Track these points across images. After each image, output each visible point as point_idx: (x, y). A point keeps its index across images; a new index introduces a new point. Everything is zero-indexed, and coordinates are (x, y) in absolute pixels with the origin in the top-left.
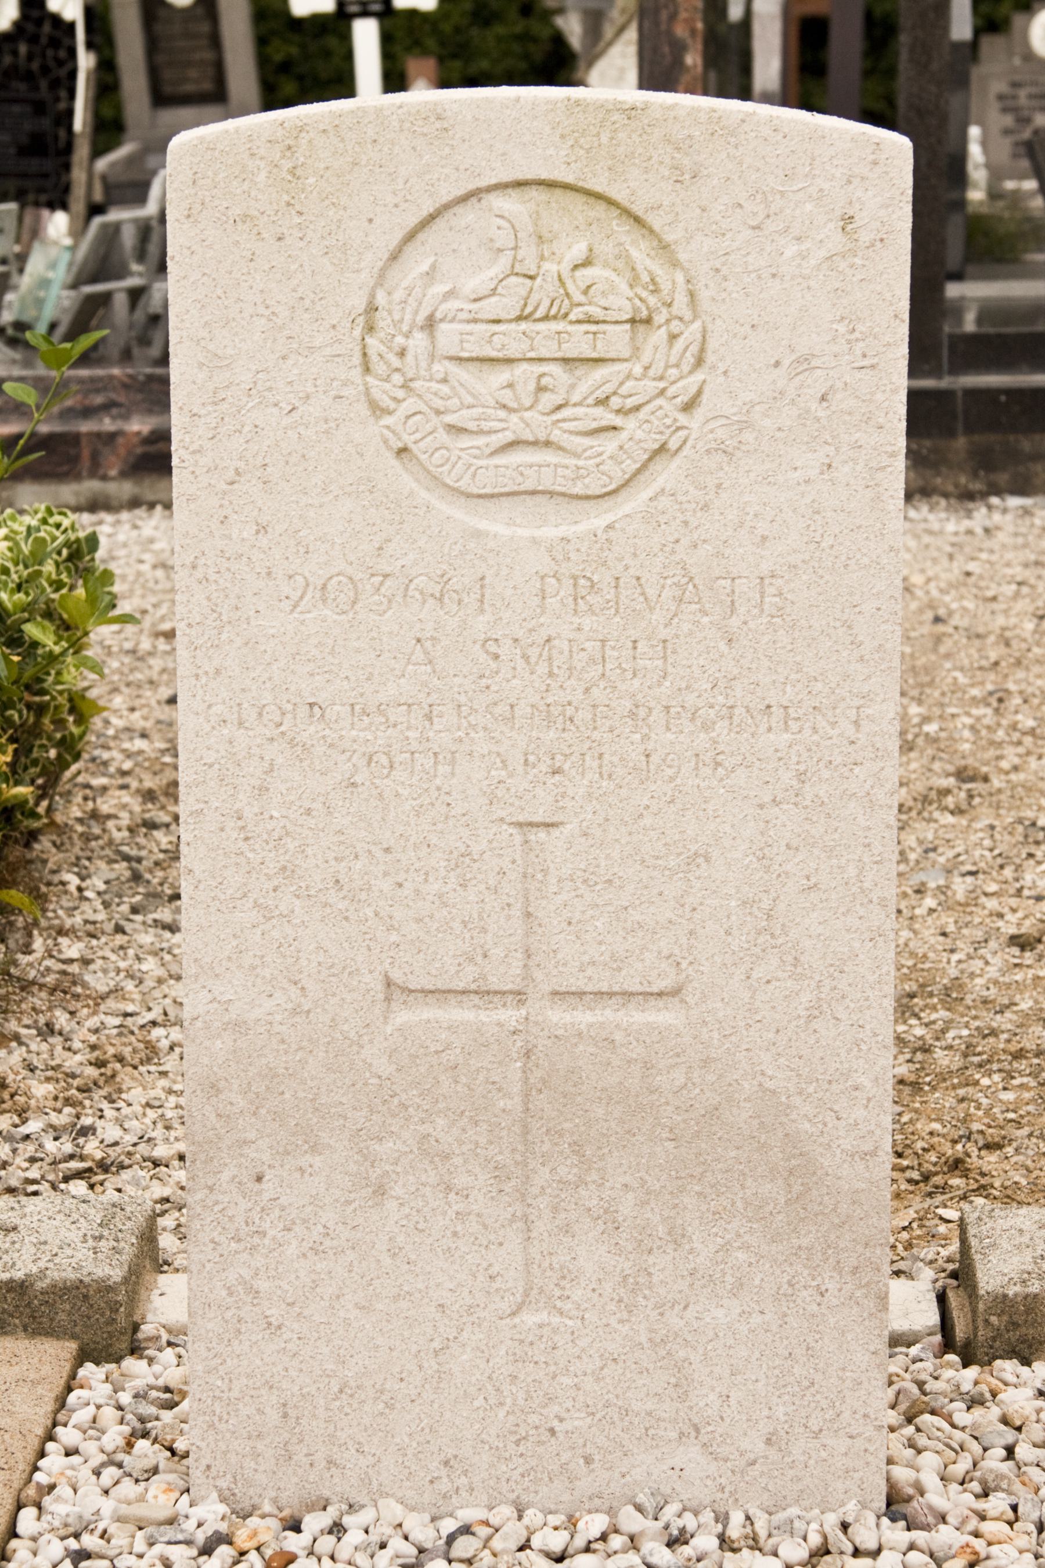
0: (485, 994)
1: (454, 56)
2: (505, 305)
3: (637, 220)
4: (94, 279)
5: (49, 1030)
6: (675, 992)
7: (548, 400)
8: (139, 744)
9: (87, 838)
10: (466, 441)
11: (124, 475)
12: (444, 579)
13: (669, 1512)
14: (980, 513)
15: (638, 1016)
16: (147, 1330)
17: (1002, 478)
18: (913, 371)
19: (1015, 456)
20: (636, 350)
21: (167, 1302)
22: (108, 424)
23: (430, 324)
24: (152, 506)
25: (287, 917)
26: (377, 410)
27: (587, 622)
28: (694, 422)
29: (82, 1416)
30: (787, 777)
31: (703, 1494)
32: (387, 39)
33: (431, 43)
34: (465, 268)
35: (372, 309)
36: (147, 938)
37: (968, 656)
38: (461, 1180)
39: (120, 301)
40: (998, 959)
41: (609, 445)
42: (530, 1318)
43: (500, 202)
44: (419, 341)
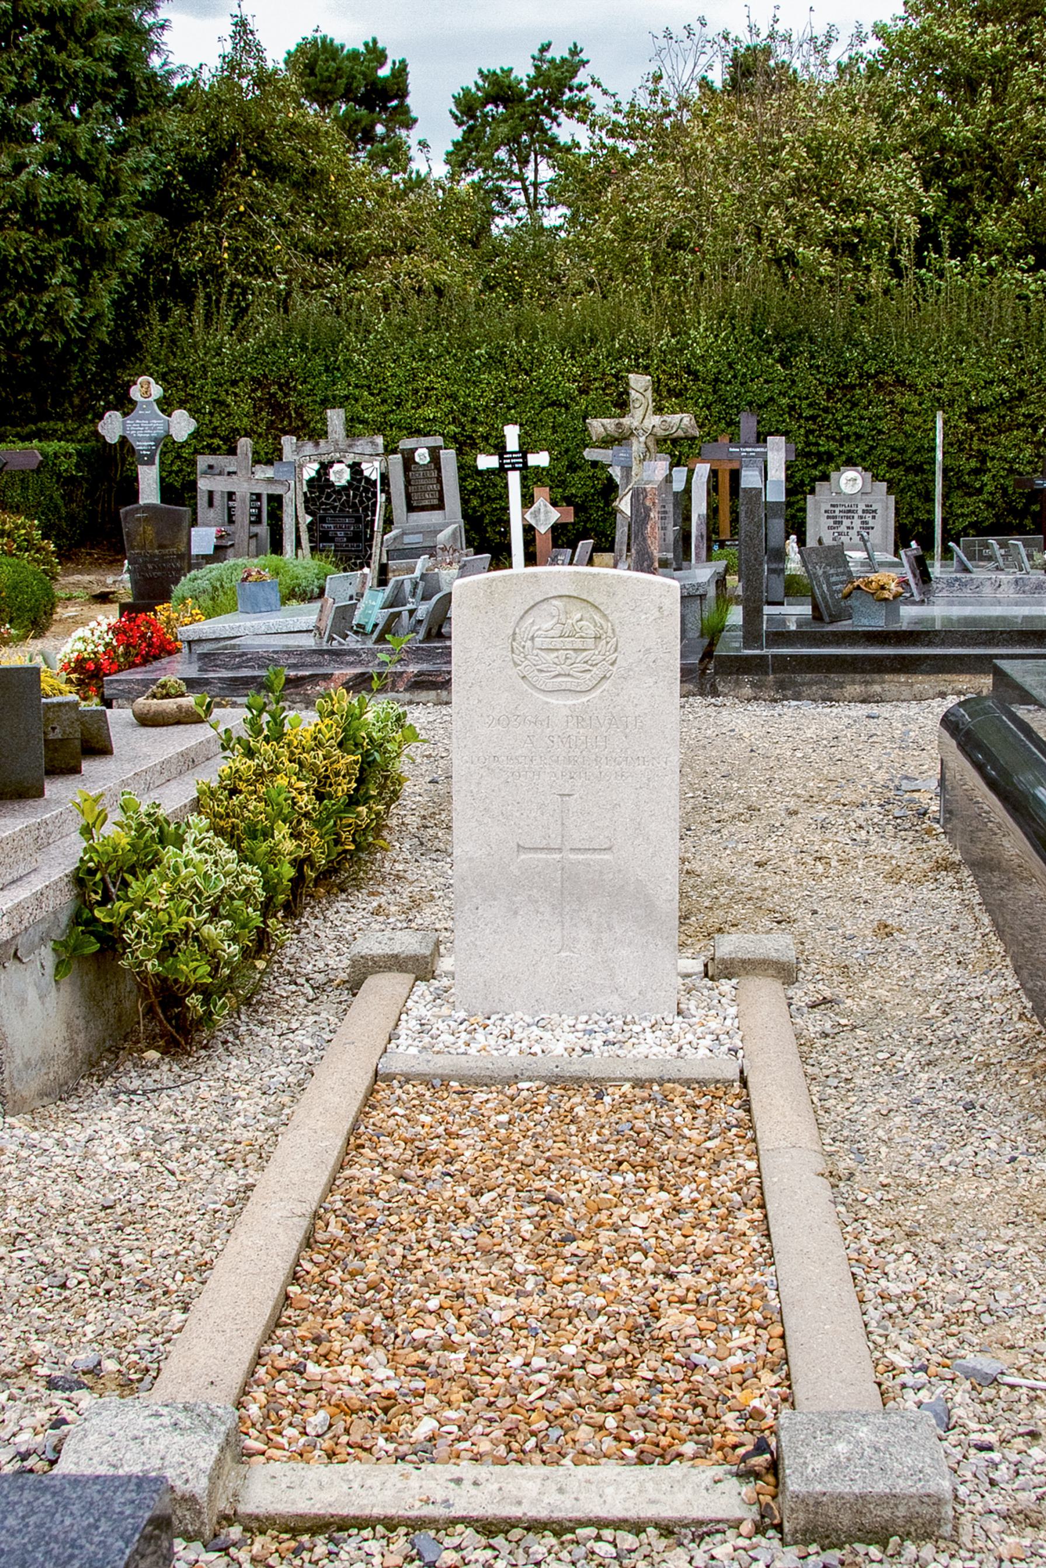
0: (549, 849)
1: (558, 487)
2: (556, 632)
4: (391, 606)
5: (394, 892)
6: (610, 849)
7: (569, 662)
8: (418, 798)
9: (400, 832)
11: (406, 690)
12: (536, 717)
13: (608, 1015)
14: (779, 708)
15: (597, 856)
16: (437, 972)
17: (789, 693)
19: (795, 684)
20: (596, 647)
21: (445, 964)
22: (399, 668)
23: (533, 638)
24: (418, 703)
25: (486, 824)
26: (516, 665)
28: (614, 669)
29: (419, 993)
30: (645, 780)
31: (619, 1010)
32: (524, 478)
33: (547, 480)
34: (543, 623)
35: (514, 634)
36: (428, 864)
37: (762, 764)
39: (405, 615)
40: (750, 869)
41: (588, 676)
42: (563, 954)
43: (554, 602)
44: (529, 643)
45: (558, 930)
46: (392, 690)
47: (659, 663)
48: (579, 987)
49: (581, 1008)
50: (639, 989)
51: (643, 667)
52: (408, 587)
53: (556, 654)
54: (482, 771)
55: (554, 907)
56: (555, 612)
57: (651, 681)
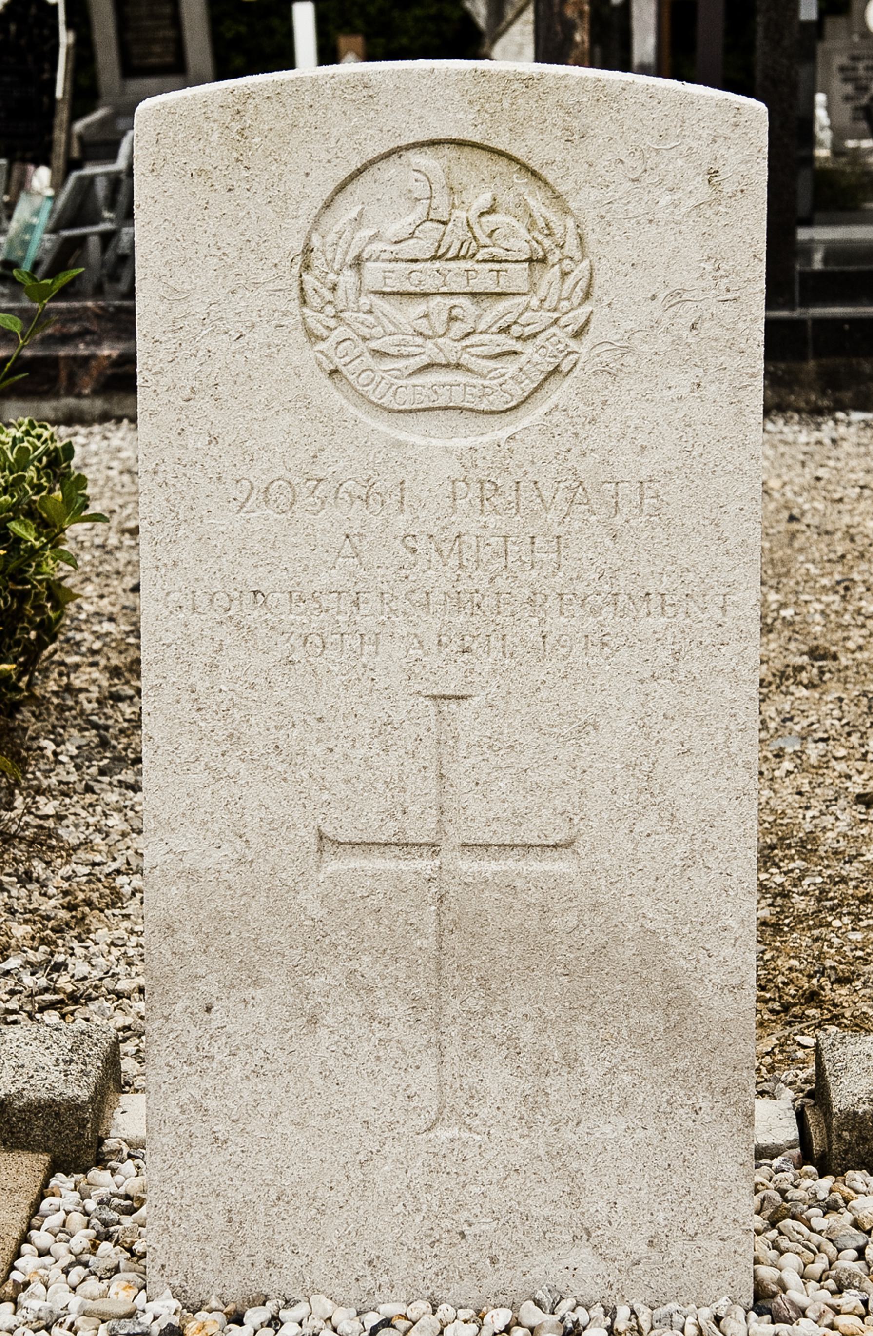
2: (422, 247)
3: (534, 173)
5: (26, 878)
6: (569, 844)
7: (458, 329)
8: (107, 627)
10: (388, 364)
11: (95, 393)
16: (111, 1144)
17: (847, 396)
18: (769, 306)
21: (128, 1119)
22: (82, 350)
23: (358, 263)
24: (119, 420)
26: (313, 337)
27: (492, 520)
28: (583, 347)
30: (664, 656)
34: (389, 216)
35: (308, 250)
36: (112, 797)
37: (819, 549)
38: (384, 1011)
39: (94, 243)
41: (510, 367)
42: (443, 1134)
43: (416, 158)
44: (348, 277)
45: (429, 1062)
46: (69, 393)
47: (708, 329)
48: (485, 1225)
49: (492, 1282)
50: (647, 1231)
51: (663, 342)
52: (101, 188)
53: (419, 307)
54: (221, 633)
55: (416, 1005)
56: (420, 190)
57: (683, 382)
